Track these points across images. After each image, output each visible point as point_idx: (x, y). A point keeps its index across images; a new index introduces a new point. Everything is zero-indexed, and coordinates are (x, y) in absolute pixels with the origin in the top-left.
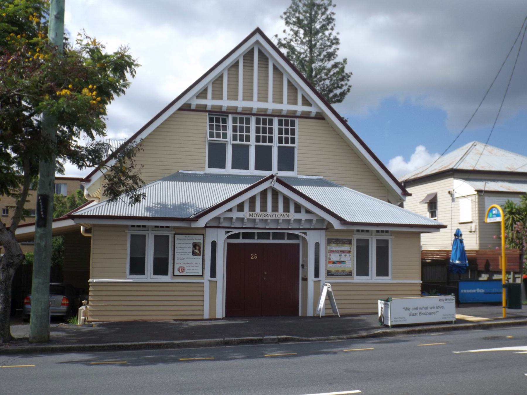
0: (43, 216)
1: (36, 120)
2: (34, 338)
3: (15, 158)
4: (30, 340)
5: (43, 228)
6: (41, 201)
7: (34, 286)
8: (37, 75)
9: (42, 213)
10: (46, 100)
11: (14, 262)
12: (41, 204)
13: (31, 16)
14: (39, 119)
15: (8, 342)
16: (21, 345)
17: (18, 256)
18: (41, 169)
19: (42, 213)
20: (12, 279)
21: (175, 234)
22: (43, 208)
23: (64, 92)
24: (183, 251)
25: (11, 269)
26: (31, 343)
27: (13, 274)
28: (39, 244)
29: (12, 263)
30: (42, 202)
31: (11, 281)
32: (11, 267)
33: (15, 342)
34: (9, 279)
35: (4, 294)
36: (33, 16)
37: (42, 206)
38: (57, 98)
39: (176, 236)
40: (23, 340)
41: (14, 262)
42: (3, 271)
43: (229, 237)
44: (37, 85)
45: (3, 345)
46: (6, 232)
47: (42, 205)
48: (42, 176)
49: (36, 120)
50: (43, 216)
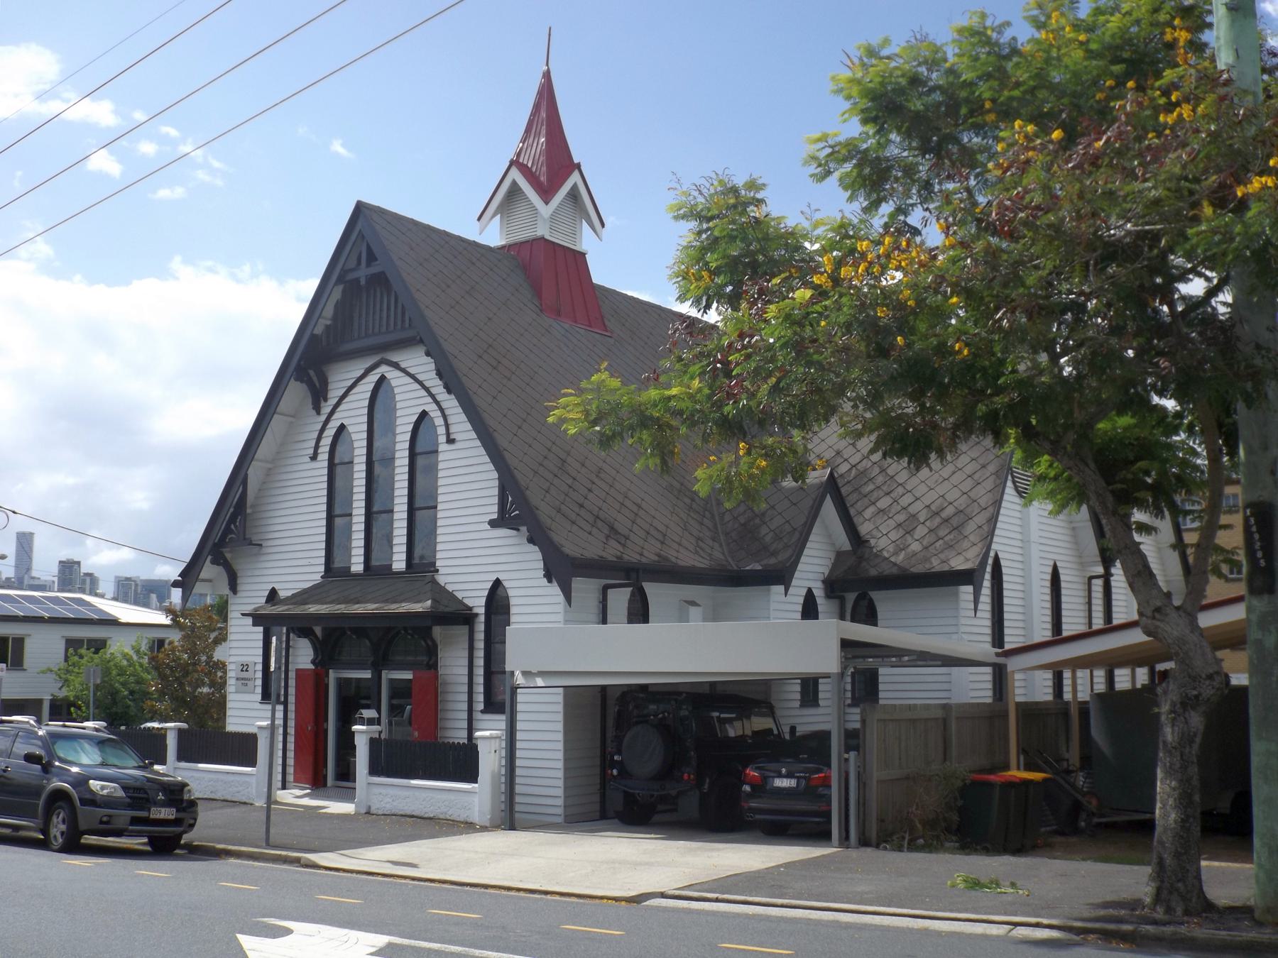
0: (1262, 563)
1: (1224, 304)
2: (1268, 910)
3: (1179, 415)
4: (1257, 914)
5: (1266, 597)
6: (1252, 520)
7: (1256, 761)
8: (1174, 162)
9: (1260, 554)
10: (1208, 220)
11: (1200, 694)
12: (1254, 529)
13: (1168, 30)
14: (1229, 299)
15: (1198, 915)
16: (1229, 930)
17: (1210, 677)
18: (1243, 432)
19: (1260, 554)
20: (1198, 740)
21: (605, 588)
22: (1261, 539)
23: (1256, 184)
24: (1111, 911)
25: (1193, 713)
26: (1260, 924)
27: (1201, 728)
28: (1259, 643)
29: (1197, 697)
30: (1256, 523)
31: (1196, 747)
32: (1193, 708)
33: (1216, 916)
34: (1191, 742)
35: (1181, 781)
36: (1174, 28)
37: (1257, 536)
38: (1242, 206)
39: (610, 591)
40: (1242, 912)
41: (1200, 694)
42: (1174, 719)
43: (997, 655)
44: (1178, 190)
45: (1182, 923)
46: (1174, 615)
47: (1258, 531)
48: (1249, 452)
49: (1224, 304)
50: (1262, 563)
